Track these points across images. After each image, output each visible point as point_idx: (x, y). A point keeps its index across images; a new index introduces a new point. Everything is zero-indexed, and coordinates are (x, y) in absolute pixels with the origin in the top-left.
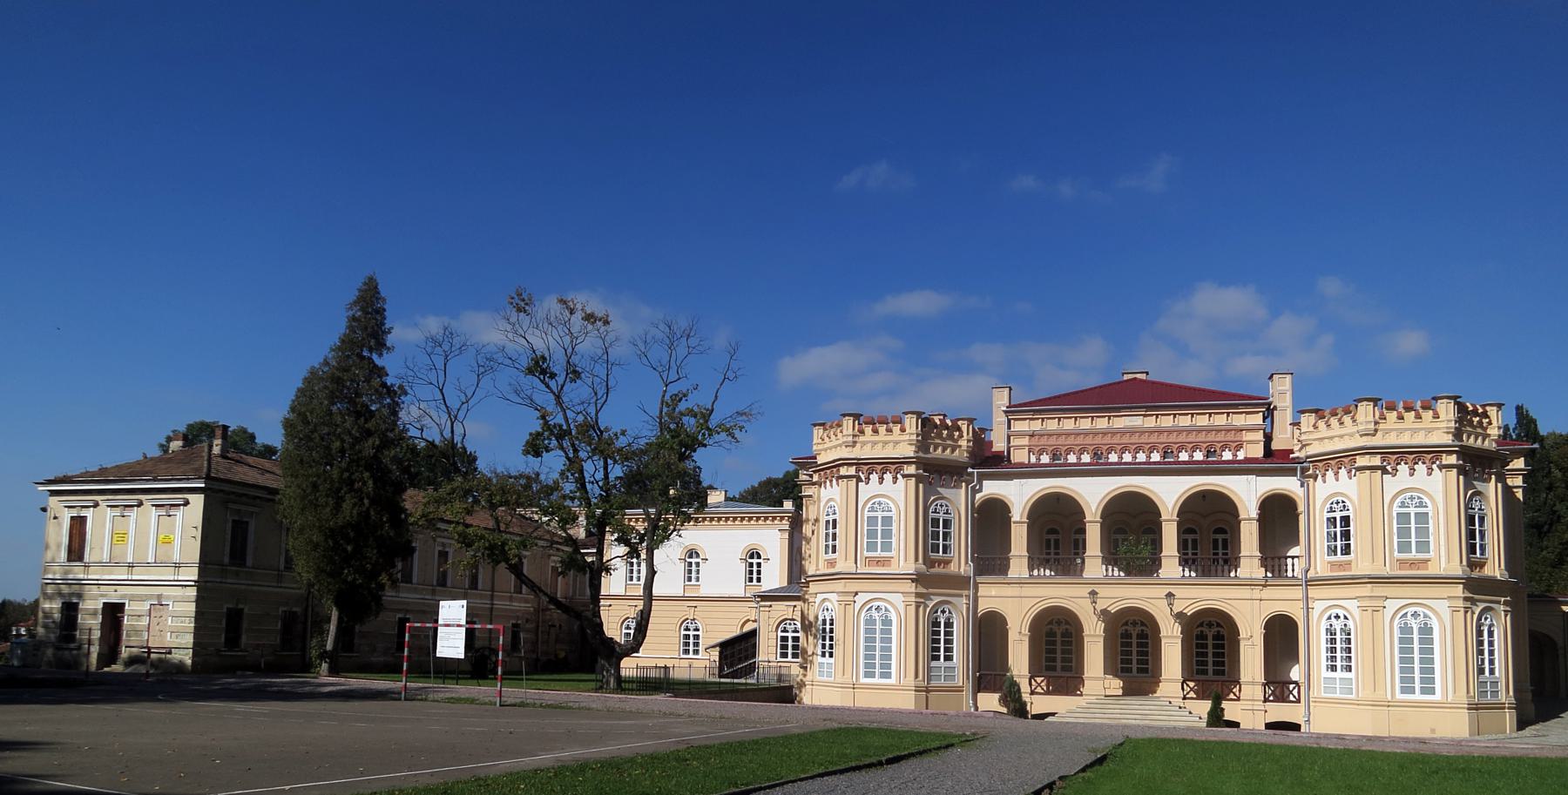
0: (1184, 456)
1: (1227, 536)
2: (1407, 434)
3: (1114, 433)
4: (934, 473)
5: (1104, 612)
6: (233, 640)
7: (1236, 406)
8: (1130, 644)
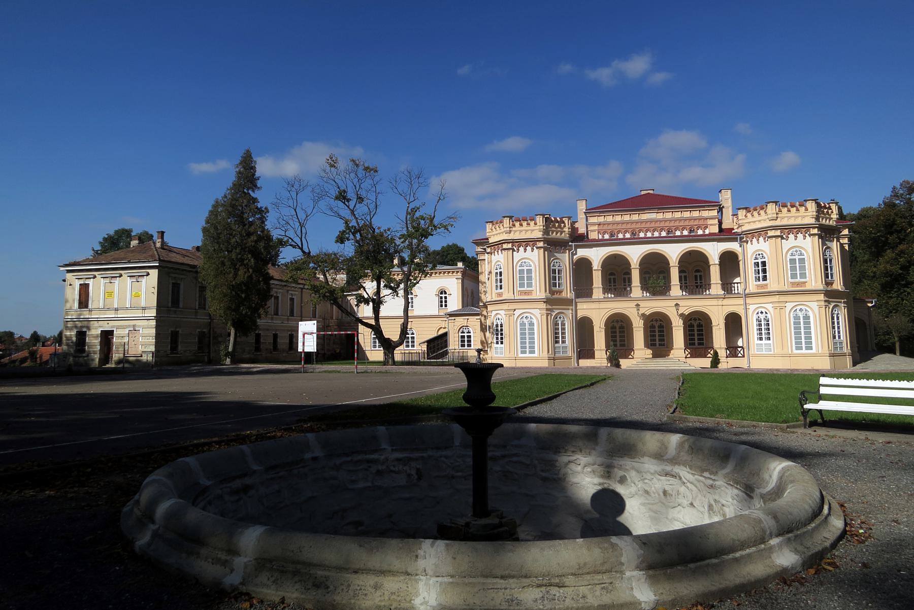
0: (678, 233)
3: (642, 222)
4: (553, 246)
5: (643, 315)
6: (174, 348)
7: (703, 207)
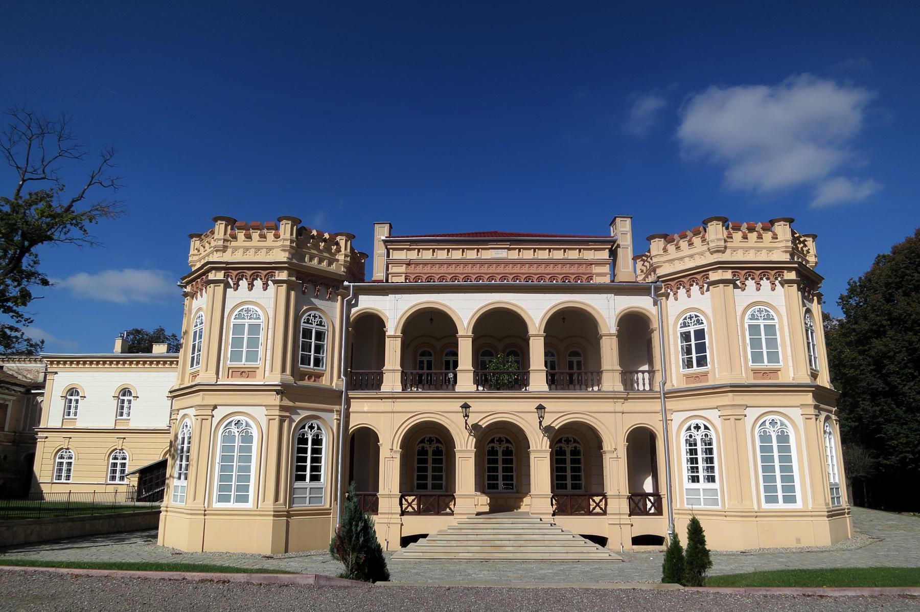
1: (581, 359)
2: (752, 252)
3: (482, 263)
4: (307, 282)
5: (476, 427)
8: (496, 461)
